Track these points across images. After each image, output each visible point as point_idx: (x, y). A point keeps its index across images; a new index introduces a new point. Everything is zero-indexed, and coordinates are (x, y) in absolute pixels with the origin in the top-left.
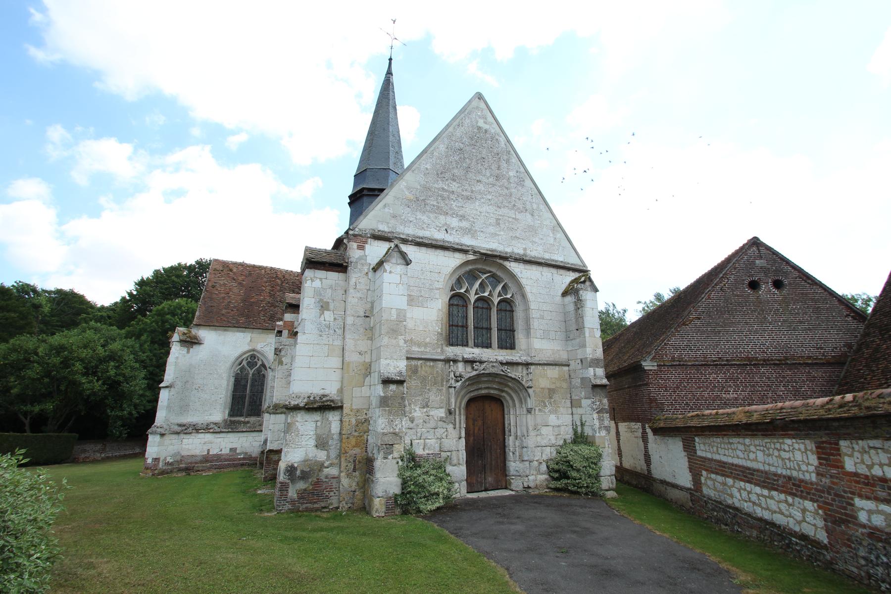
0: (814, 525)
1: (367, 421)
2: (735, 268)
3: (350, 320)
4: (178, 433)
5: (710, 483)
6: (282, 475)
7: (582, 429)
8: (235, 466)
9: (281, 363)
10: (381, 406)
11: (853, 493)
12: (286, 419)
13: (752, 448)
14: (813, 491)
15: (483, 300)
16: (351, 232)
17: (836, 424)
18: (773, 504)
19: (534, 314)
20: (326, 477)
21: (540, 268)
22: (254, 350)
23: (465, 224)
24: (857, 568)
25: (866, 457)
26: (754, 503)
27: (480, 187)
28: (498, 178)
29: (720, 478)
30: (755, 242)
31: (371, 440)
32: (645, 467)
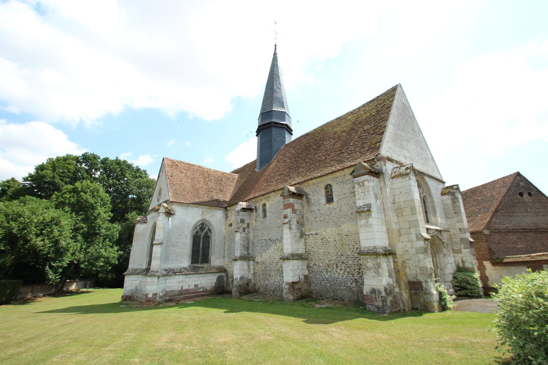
4: (164, 276)
22: (203, 220)
30: (518, 174)
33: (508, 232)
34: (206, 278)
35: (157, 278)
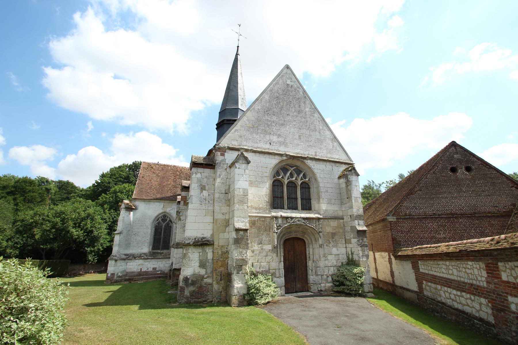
0: (487, 313)
1: (227, 252)
2: (442, 160)
3: (217, 195)
4: (124, 259)
5: (428, 288)
6: (181, 282)
7: (352, 256)
8: (155, 278)
9: (180, 219)
10: (235, 244)
11: (507, 293)
12: (183, 251)
13: (451, 267)
14: (485, 292)
15: (292, 184)
16: (217, 146)
17: (495, 253)
18: (463, 301)
19: (322, 190)
20: (205, 284)
21: (325, 163)
22: (165, 212)
23: (281, 139)
24: (511, 337)
25: (513, 272)
26: (453, 300)
27: (289, 118)
28: (299, 112)
29: (433, 285)
30: (453, 144)
31: (230, 263)
32: (391, 279)
33: (426, 217)
34: (164, 262)
35: (114, 261)
